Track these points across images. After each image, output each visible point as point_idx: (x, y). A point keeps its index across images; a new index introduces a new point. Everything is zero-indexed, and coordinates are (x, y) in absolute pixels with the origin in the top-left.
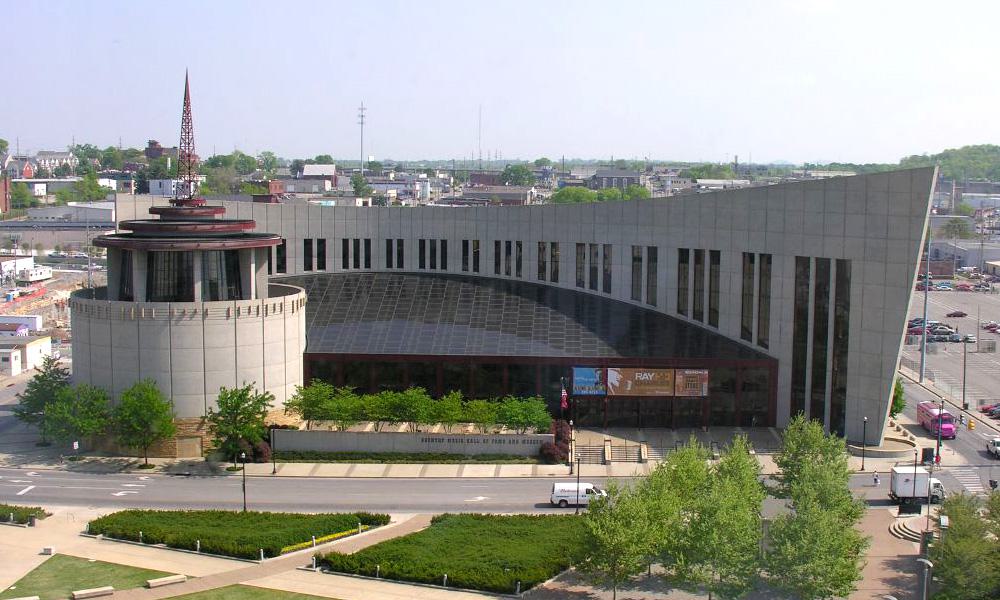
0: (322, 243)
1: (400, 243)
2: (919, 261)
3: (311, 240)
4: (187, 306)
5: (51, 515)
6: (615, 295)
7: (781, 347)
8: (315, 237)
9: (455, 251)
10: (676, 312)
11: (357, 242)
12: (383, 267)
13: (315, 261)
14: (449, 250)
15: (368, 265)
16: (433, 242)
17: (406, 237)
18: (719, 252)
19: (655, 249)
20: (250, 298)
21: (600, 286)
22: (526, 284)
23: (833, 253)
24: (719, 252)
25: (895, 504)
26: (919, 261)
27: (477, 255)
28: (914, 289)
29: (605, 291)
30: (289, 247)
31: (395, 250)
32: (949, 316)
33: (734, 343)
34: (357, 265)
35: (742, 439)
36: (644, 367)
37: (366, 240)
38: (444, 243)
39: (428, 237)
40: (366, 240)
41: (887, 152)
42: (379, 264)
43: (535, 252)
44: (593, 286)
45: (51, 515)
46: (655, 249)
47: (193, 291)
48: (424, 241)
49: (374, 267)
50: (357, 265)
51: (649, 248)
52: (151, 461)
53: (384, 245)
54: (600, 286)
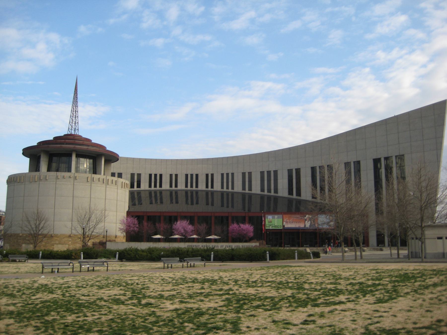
4: (67, 174)
6: (280, 194)
10: (311, 198)
11: (228, 174)
12: (147, 188)
13: (136, 184)
16: (192, 175)
20: (100, 174)
21: (272, 191)
22: (236, 192)
25: (176, 256)
27: (250, 181)
29: (268, 192)
30: (169, 201)
32: (116, 185)
35: (34, 231)
37: (296, 169)
38: (197, 175)
39: (189, 173)
40: (296, 169)
42: (166, 186)
44: (269, 191)
47: (245, 179)
48: (292, 170)
49: (179, 187)
50: (155, 186)
54: (272, 191)
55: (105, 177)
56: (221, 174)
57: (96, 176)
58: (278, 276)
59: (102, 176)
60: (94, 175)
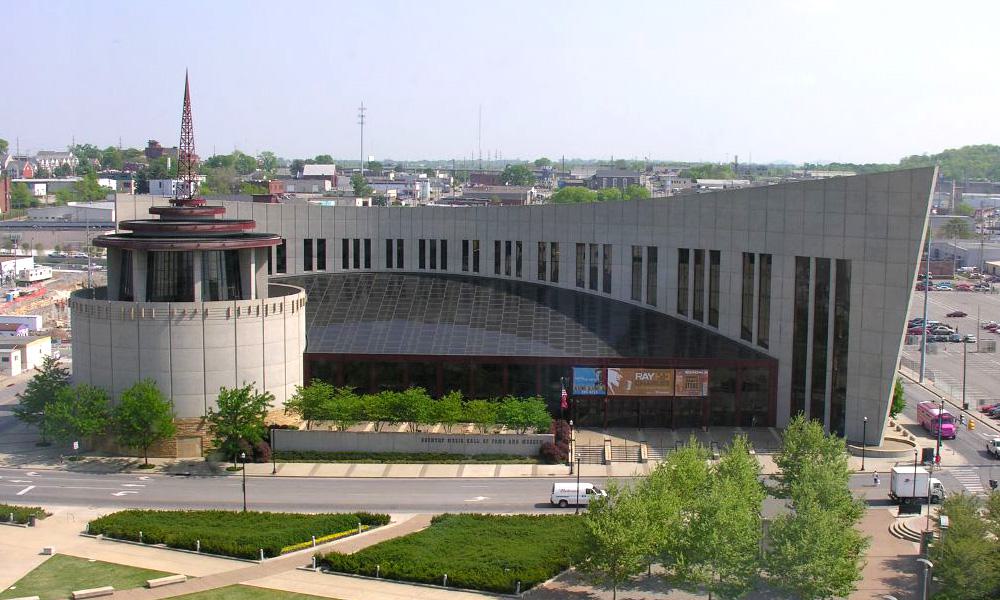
0: (322, 243)
1: (400, 243)
2: (919, 261)
3: (311, 240)
4: (187, 306)
5: (51, 515)
6: (615, 295)
7: (781, 347)
8: (315, 237)
9: (455, 251)
11: (357, 242)
12: (383, 267)
13: (315, 261)
14: (449, 250)
15: (368, 265)
16: (433, 242)
17: (406, 237)
18: (719, 252)
19: (655, 249)
21: (600, 286)
22: (526, 284)
23: (833, 253)
24: (719, 252)
26: (919, 261)
27: (477, 255)
28: (914, 289)
29: (605, 291)
30: (289, 247)
31: (395, 250)
32: (949, 316)
33: (734, 343)
34: (357, 265)
36: (644, 367)
37: (366, 240)
38: (444, 243)
40: (366, 240)
41: (887, 152)
42: (379, 264)
43: (535, 252)
44: (593, 286)
45: (51, 515)
46: (655, 249)
48: (424, 241)
49: (374, 267)
50: (357, 265)
51: (649, 248)
52: (151, 461)
53: (384, 245)
54: (600, 286)
55: (259, 302)
56: (387, 240)
57: (243, 304)
58: (41, 197)
59: (253, 302)
60: (240, 303)
